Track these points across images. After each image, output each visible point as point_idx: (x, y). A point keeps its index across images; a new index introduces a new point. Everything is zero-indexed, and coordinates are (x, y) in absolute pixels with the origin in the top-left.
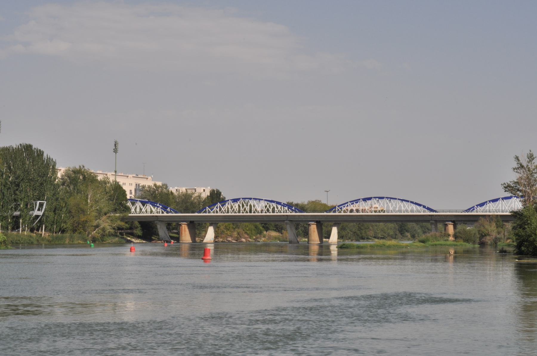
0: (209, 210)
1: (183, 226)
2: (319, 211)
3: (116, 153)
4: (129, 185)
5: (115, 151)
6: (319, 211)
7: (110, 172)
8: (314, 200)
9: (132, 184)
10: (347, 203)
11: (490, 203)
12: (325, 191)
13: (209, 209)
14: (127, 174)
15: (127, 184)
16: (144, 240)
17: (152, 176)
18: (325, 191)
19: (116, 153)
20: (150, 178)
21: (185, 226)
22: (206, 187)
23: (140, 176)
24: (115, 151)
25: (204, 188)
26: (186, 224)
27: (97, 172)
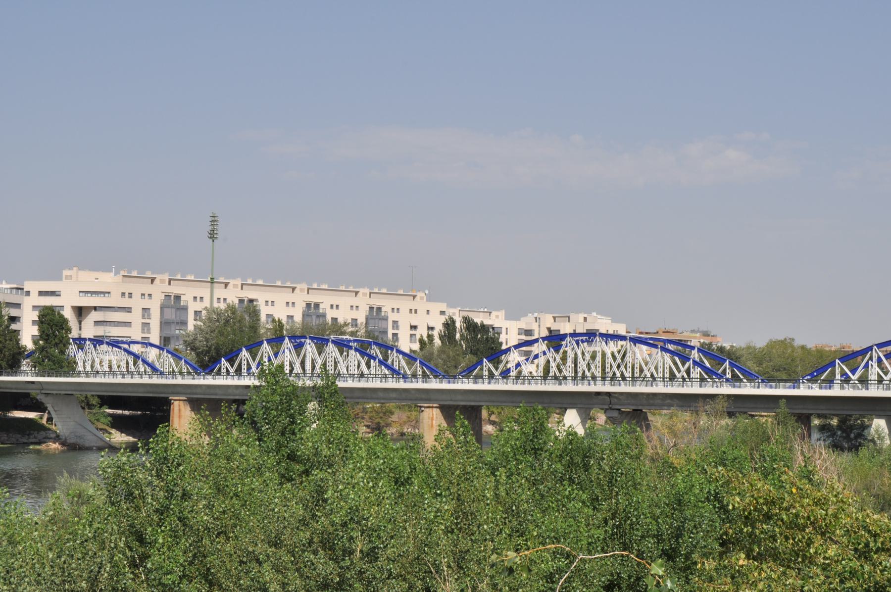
0: (843, 374)
1: (176, 403)
2: (394, 395)
3: (213, 241)
4: (426, 312)
5: (212, 236)
6: (394, 395)
7: (234, 278)
8: (781, 338)
9: (398, 309)
10: (870, 348)
11: (510, 368)
12: (214, 219)
13: (844, 367)
14: (409, 292)
15: (405, 310)
16: (128, 435)
17: (427, 292)
18: (214, 219)
19: (213, 241)
20: (420, 295)
21: (179, 405)
22: (590, 313)
23: (189, 278)
24: (212, 236)
25: (586, 316)
26: (185, 400)
27: (398, 293)
